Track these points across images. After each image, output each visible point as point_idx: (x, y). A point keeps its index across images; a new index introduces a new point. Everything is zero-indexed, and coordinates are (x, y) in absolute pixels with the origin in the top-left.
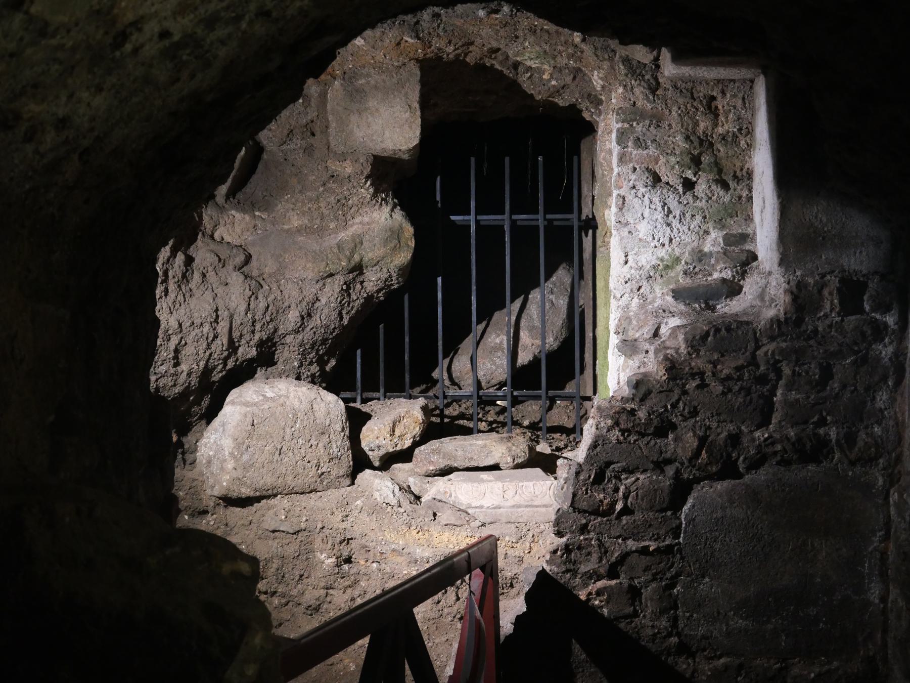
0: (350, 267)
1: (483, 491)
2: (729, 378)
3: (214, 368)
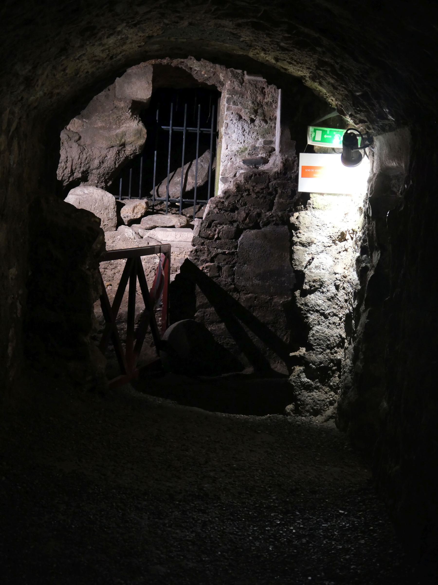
0: (120, 144)
2: (258, 192)
3: (65, 180)
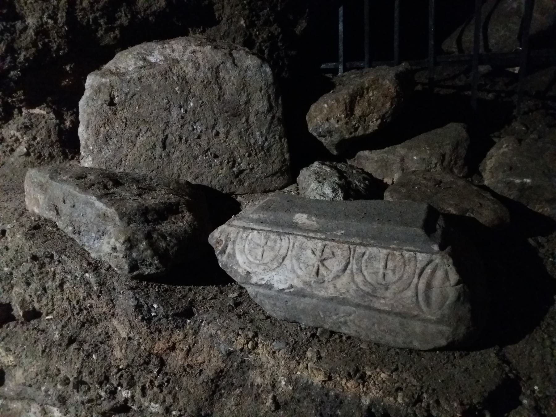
1: (283, 252)
